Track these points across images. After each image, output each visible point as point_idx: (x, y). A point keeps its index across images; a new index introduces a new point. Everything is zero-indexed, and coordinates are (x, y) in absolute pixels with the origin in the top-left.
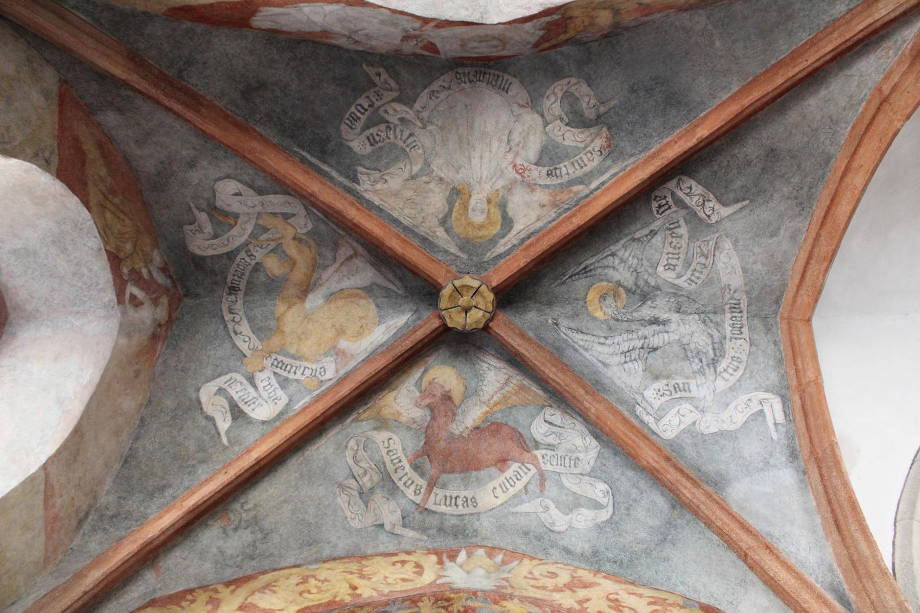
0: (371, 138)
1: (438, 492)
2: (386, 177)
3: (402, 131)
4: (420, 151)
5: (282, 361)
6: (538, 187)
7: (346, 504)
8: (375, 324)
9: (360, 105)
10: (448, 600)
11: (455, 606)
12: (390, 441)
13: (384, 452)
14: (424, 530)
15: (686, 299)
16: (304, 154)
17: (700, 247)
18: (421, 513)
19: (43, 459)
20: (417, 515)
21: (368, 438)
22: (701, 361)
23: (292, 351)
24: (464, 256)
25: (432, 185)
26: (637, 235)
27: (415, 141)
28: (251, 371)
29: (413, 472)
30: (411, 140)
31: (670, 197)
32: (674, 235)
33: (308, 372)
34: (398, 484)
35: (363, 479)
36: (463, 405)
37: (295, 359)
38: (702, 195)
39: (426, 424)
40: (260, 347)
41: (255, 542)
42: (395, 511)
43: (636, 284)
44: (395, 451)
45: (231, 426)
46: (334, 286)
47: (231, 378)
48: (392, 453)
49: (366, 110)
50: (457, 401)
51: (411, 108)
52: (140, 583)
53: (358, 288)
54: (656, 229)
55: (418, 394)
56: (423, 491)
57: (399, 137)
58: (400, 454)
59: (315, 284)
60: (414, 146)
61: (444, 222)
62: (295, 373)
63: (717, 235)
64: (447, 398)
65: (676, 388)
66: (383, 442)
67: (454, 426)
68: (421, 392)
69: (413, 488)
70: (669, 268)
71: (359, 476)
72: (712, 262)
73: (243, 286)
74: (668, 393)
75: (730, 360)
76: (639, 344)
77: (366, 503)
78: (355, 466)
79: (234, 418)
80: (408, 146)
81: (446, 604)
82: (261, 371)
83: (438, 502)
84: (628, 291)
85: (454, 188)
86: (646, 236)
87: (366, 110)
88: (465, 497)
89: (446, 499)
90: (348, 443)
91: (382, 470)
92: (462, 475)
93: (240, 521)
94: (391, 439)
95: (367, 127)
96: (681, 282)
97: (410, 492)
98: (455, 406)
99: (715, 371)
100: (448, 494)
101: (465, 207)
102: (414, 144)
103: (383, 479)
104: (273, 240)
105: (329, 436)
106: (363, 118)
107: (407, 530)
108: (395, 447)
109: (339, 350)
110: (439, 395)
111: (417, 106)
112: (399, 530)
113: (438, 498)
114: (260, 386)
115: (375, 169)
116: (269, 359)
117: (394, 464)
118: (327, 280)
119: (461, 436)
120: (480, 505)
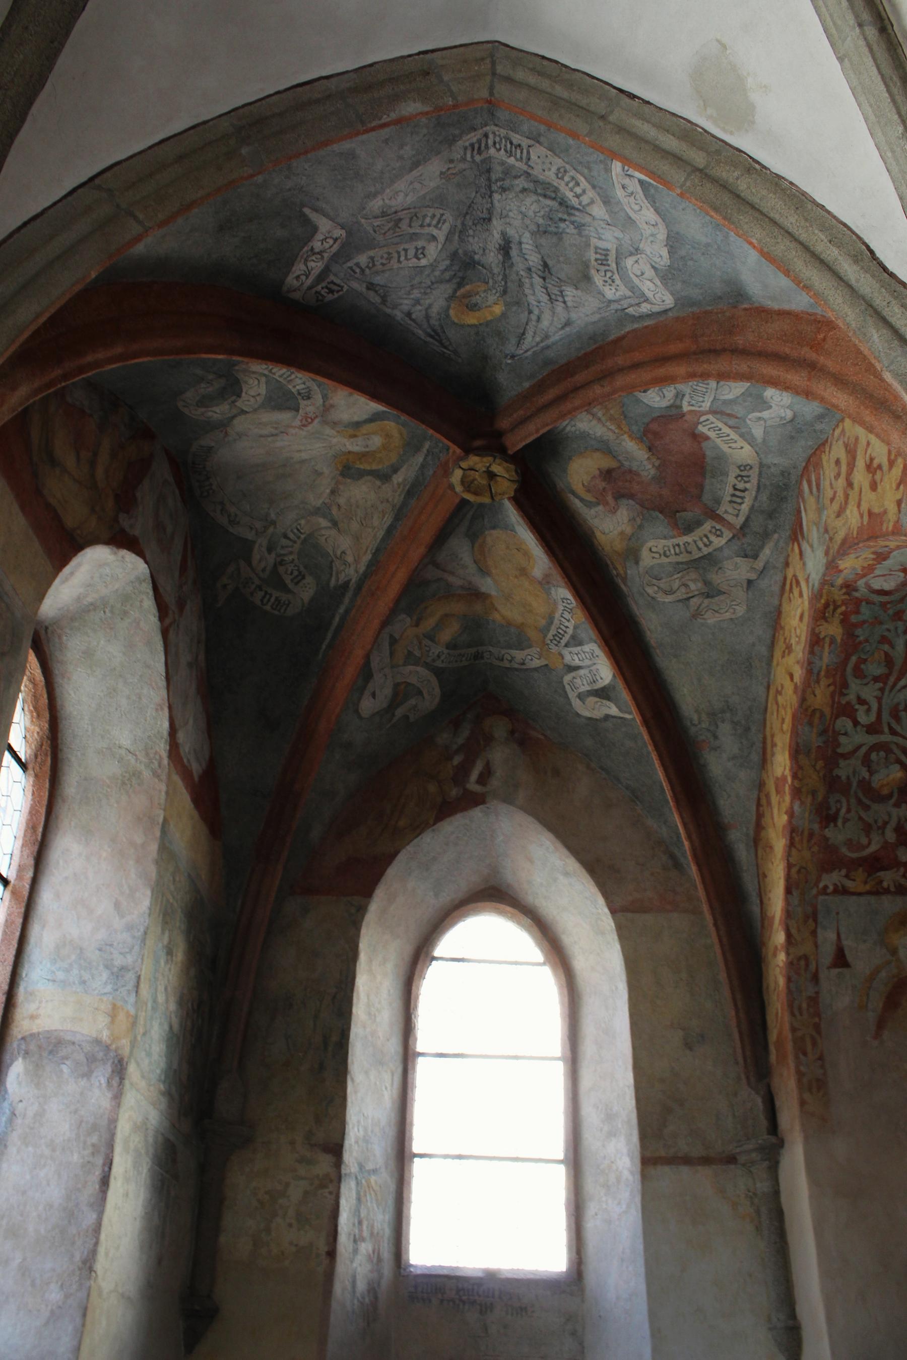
0: (296, 581)
1: (723, 510)
2: (339, 553)
3: (283, 547)
4: (303, 522)
5: (553, 636)
6: (326, 403)
7: (717, 615)
8: (515, 536)
9: (262, 601)
10: (827, 605)
11: (837, 597)
12: (653, 550)
13: (665, 560)
14: (766, 535)
15: (468, 217)
16: (324, 647)
17: (385, 234)
18: (744, 535)
19: (606, 910)
20: (745, 540)
21: (647, 573)
22: (561, 220)
23: (543, 622)
24: (427, 445)
25: (342, 501)
26: (377, 300)
27: (292, 531)
28: (561, 667)
29: (693, 534)
30: (291, 536)
31: (315, 289)
32: (371, 265)
33: (566, 615)
34: (706, 553)
35: (692, 589)
36: (620, 458)
37: (552, 623)
38: (306, 260)
39: (637, 506)
40: (538, 650)
41: (733, 722)
42: (737, 563)
43: (449, 281)
44: (666, 549)
45: (616, 704)
46: (472, 568)
47: (569, 684)
48: (668, 552)
49: (266, 593)
50: (614, 464)
51: (254, 542)
52: (736, 846)
53: (473, 547)
54: (364, 285)
55: (601, 508)
56: (718, 527)
57: (290, 549)
58: (670, 543)
59: (469, 589)
60: (298, 530)
61: (384, 477)
62: (567, 627)
63: (363, 221)
64: (607, 474)
65: (603, 262)
66: (653, 558)
67: (644, 474)
68: (598, 504)
69: (712, 538)
70: (422, 253)
71: (687, 593)
72: (405, 212)
73: (473, 650)
74: (609, 274)
75: (563, 183)
76: (537, 280)
77: (721, 593)
78: (675, 595)
79: (608, 698)
80: (299, 538)
81: (832, 607)
82: (563, 658)
83: (736, 512)
84: (460, 285)
85: (343, 474)
86: (376, 292)
87: (266, 593)
88: (736, 478)
89: (735, 502)
90: (648, 595)
91: (685, 567)
92: (708, 475)
93: (708, 730)
94: (650, 550)
95: (285, 588)
96: (441, 235)
97: (718, 542)
98: (619, 468)
99: (578, 209)
100: (729, 498)
101: (363, 456)
102: (295, 531)
103: (696, 568)
104: (420, 643)
105: (638, 614)
106: (276, 594)
107: (761, 555)
108: (660, 546)
109: (543, 579)
110: (604, 484)
111: (250, 536)
112: (759, 564)
113: (730, 510)
114: (577, 662)
115: (331, 568)
116: (550, 647)
117: (681, 553)
118: (464, 579)
119: (658, 468)
120: (750, 462)
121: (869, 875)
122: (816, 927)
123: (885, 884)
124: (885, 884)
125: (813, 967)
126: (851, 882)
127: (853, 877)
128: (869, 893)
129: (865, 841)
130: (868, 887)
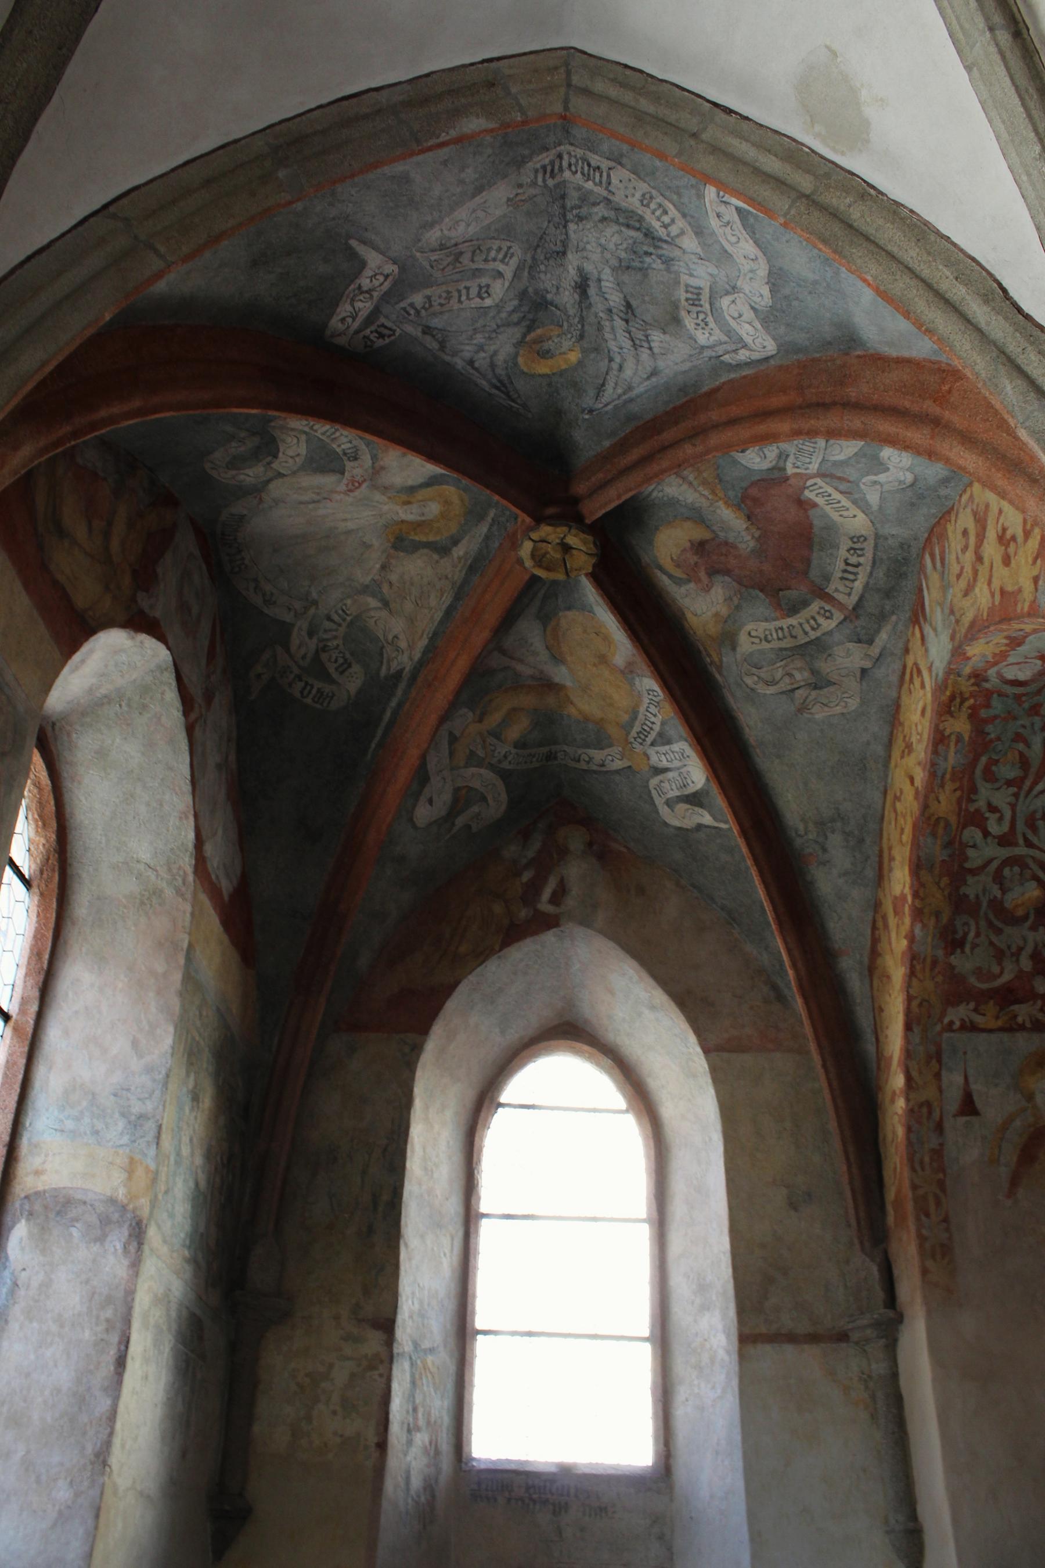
0: (341, 669)
1: (834, 587)
2: (390, 637)
3: (325, 631)
4: (349, 602)
5: (638, 733)
6: (376, 465)
7: (826, 709)
8: (593, 618)
9: (302, 692)
10: (952, 698)
11: (964, 689)
12: (752, 634)
13: (766, 646)
14: (882, 617)
15: (539, 250)
16: (373, 746)
17: (443, 269)
18: (857, 617)
19: (699, 1050)
20: (858, 623)
21: (745, 660)
22: (647, 253)
23: (626, 717)
24: (492, 513)
25: (394, 577)
26: (435, 346)
27: (336, 612)
28: (647, 769)
29: (798, 615)
30: (336, 618)
31: (363, 333)
32: (427, 305)
33: (653, 709)
34: (813, 637)
35: (797, 679)
36: (714, 528)
37: (636, 718)
38: (353, 300)
39: (734, 584)
40: (620, 749)
41: (844, 832)
42: (849, 650)
43: (517, 324)
44: (767, 633)
45: (709, 812)
46: (544, 655)
47: (655, 789)
48: (769, 637)
49: (307, 683)
50: (707, 535)
51: (293, 625)
52: (848, 975)
53: (545, 631)
54: (420, 329)
55: (692, 585)
56: (827, 608)
57: (334, 633)
58: (772, 625)
59: (541, 679)
60: (343, 611)
61: (443, 550)
62: (653, 723)
63: (418, 254)
64: (700, 547)
65: (695, 302)
66: (753, 643)
67: (742, 546)
68: (689, 581)
69: (821, 620)
70: (487, 292)
71: (792, 684)
72: (467, 244)
73: (544, 750)
74: (701, 316)
75: (648, 211)
76: (619, 323)
77: (830, 683)
78: (778, 686)
79: (701, 805)
80: (344, 620)
81: (958, 700)
82: (649, 759)
83: (848, 590)
84: (530, 329)
85: (395, 547)
86: (433, 336)
87: (307, 683)
88: (848, 551)
89: (847, 579)
90: (747, 686)
91: (790, 653)
92: (816, 548)
93: (816, 842)
94: (749, 634)
95: (328, 678)
96: (508, 271)
97: (828, 625)
98: (713, 539)
99: (666, 242)
100: (840, 575)
101: (418, 526)
102: (340, 612)
103: (802, 655)
104: (484, 741)
105: (735, 707)
106: (318, 685)
107: (877, 640)
108: (761, 630)
109: (626, 667)
110: (696, 558)
111: (288, 618)
112: (875, 650)
113: (841, 588)
114: (665, 763)
115: (381, 655)
116: (634, 746)
117: (785, 637)
118: (535, 668)
119: (758, 540)
120: (864, 533)
121: (1001, 1009)
122: (940, 1069)
123: (1020, 1020)
124: (1020, 1020)
125: (936, 1115)
126: (981, 1017)
127: (982, 1012)
128: (1001, 1029)
129: (996, 970)
130: (1000, 1023)
